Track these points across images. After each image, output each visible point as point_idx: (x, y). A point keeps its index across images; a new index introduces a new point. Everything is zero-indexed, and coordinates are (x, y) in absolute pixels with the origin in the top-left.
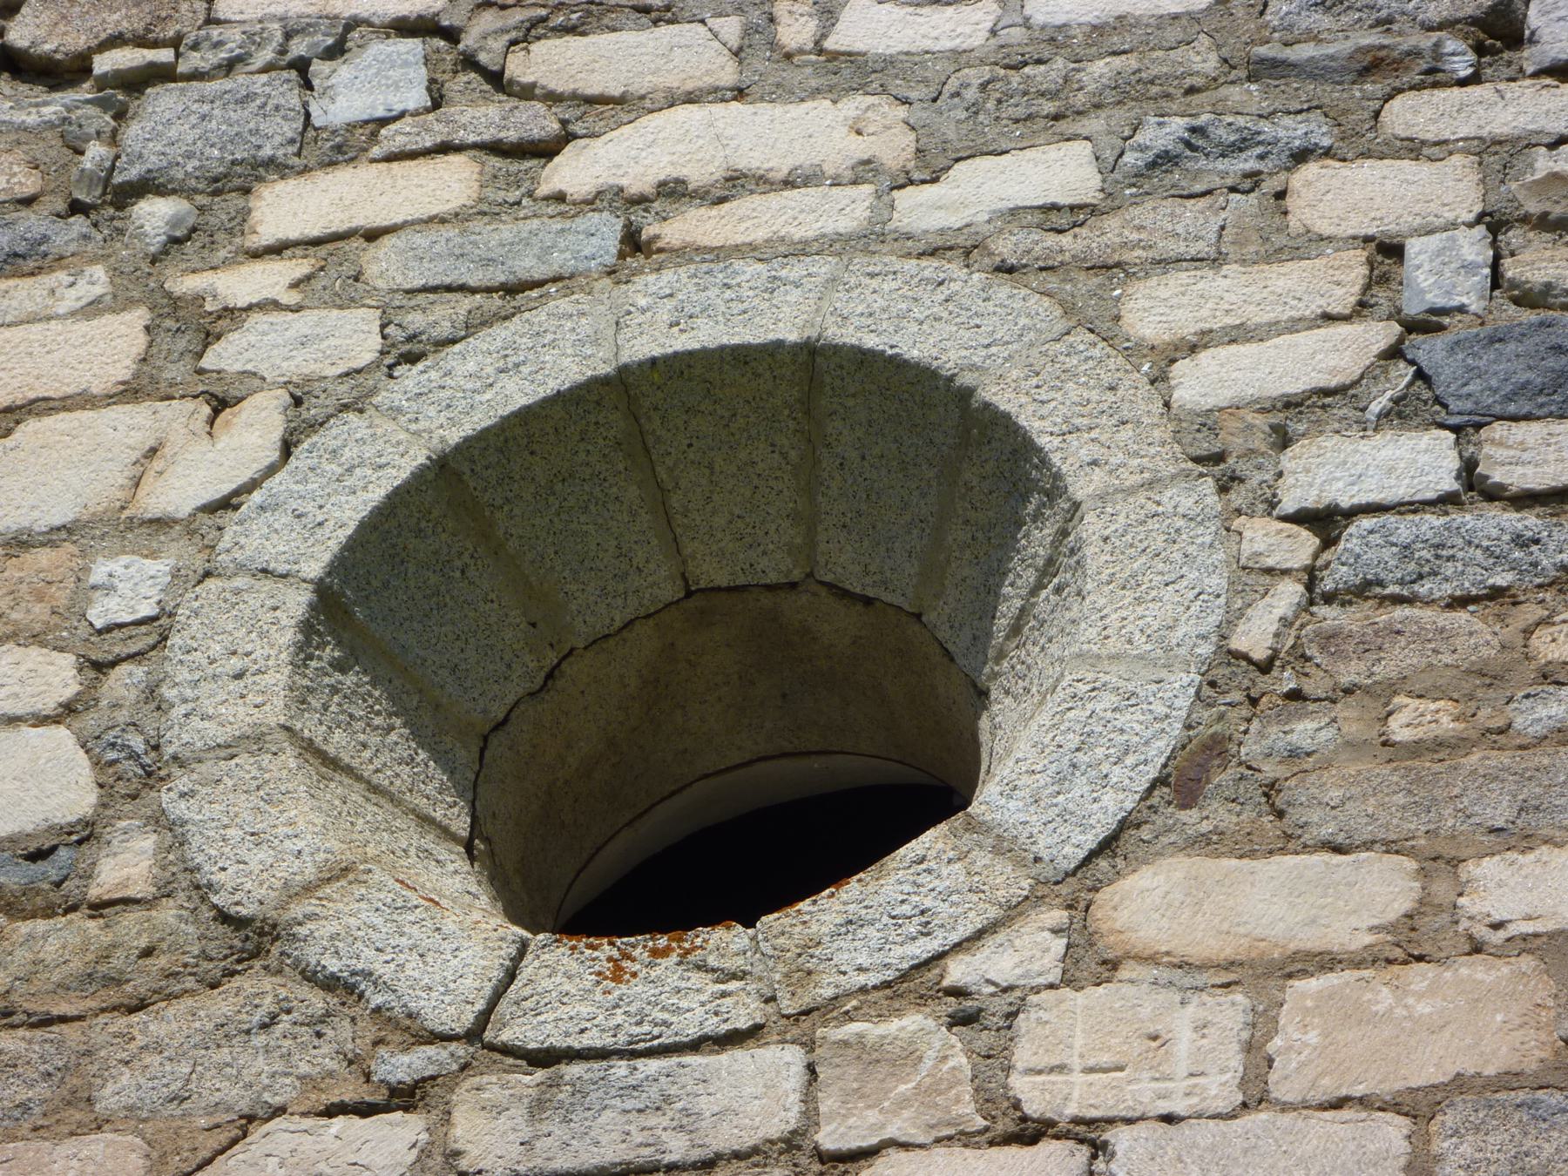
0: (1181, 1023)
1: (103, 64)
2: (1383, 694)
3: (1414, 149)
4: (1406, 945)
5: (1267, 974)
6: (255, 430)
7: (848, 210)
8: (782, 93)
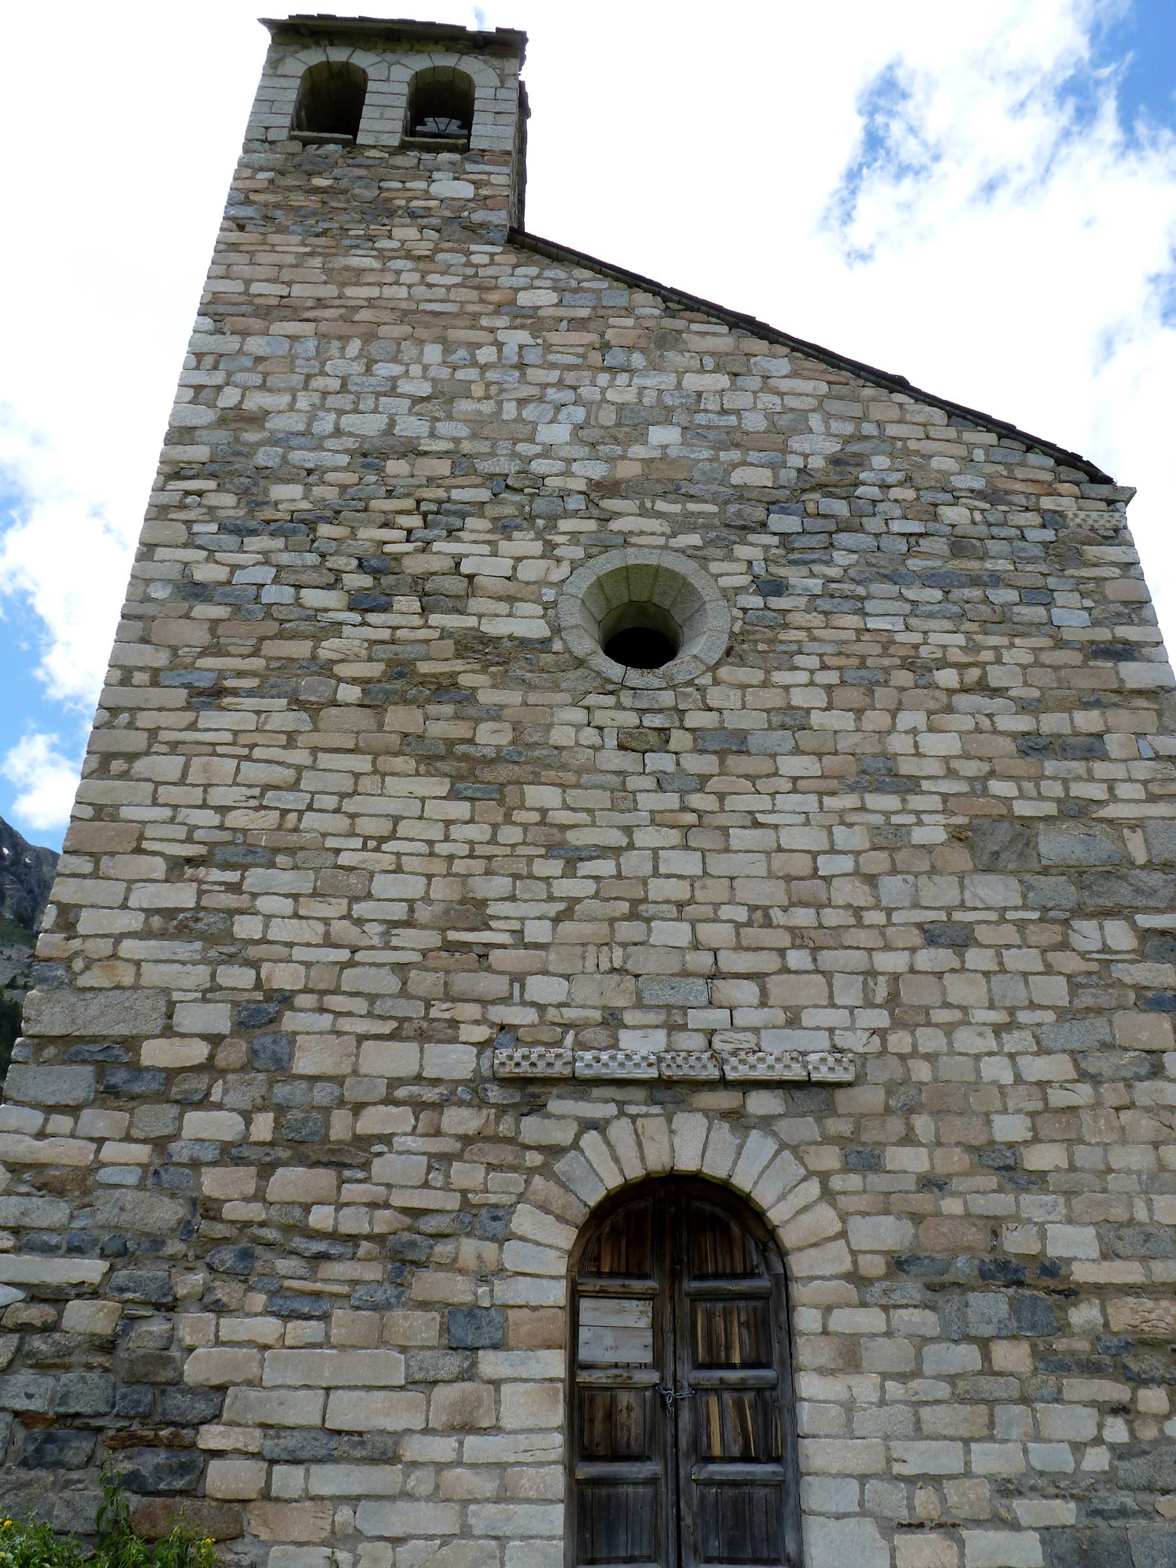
0: (731, 693)
1: (527, 491)
2: (756, 642)
3: (752, 544)
4: (765, 684)
5: (743, 687)
6: (565, 569)
7: (661, 541)
8: (647, 517)
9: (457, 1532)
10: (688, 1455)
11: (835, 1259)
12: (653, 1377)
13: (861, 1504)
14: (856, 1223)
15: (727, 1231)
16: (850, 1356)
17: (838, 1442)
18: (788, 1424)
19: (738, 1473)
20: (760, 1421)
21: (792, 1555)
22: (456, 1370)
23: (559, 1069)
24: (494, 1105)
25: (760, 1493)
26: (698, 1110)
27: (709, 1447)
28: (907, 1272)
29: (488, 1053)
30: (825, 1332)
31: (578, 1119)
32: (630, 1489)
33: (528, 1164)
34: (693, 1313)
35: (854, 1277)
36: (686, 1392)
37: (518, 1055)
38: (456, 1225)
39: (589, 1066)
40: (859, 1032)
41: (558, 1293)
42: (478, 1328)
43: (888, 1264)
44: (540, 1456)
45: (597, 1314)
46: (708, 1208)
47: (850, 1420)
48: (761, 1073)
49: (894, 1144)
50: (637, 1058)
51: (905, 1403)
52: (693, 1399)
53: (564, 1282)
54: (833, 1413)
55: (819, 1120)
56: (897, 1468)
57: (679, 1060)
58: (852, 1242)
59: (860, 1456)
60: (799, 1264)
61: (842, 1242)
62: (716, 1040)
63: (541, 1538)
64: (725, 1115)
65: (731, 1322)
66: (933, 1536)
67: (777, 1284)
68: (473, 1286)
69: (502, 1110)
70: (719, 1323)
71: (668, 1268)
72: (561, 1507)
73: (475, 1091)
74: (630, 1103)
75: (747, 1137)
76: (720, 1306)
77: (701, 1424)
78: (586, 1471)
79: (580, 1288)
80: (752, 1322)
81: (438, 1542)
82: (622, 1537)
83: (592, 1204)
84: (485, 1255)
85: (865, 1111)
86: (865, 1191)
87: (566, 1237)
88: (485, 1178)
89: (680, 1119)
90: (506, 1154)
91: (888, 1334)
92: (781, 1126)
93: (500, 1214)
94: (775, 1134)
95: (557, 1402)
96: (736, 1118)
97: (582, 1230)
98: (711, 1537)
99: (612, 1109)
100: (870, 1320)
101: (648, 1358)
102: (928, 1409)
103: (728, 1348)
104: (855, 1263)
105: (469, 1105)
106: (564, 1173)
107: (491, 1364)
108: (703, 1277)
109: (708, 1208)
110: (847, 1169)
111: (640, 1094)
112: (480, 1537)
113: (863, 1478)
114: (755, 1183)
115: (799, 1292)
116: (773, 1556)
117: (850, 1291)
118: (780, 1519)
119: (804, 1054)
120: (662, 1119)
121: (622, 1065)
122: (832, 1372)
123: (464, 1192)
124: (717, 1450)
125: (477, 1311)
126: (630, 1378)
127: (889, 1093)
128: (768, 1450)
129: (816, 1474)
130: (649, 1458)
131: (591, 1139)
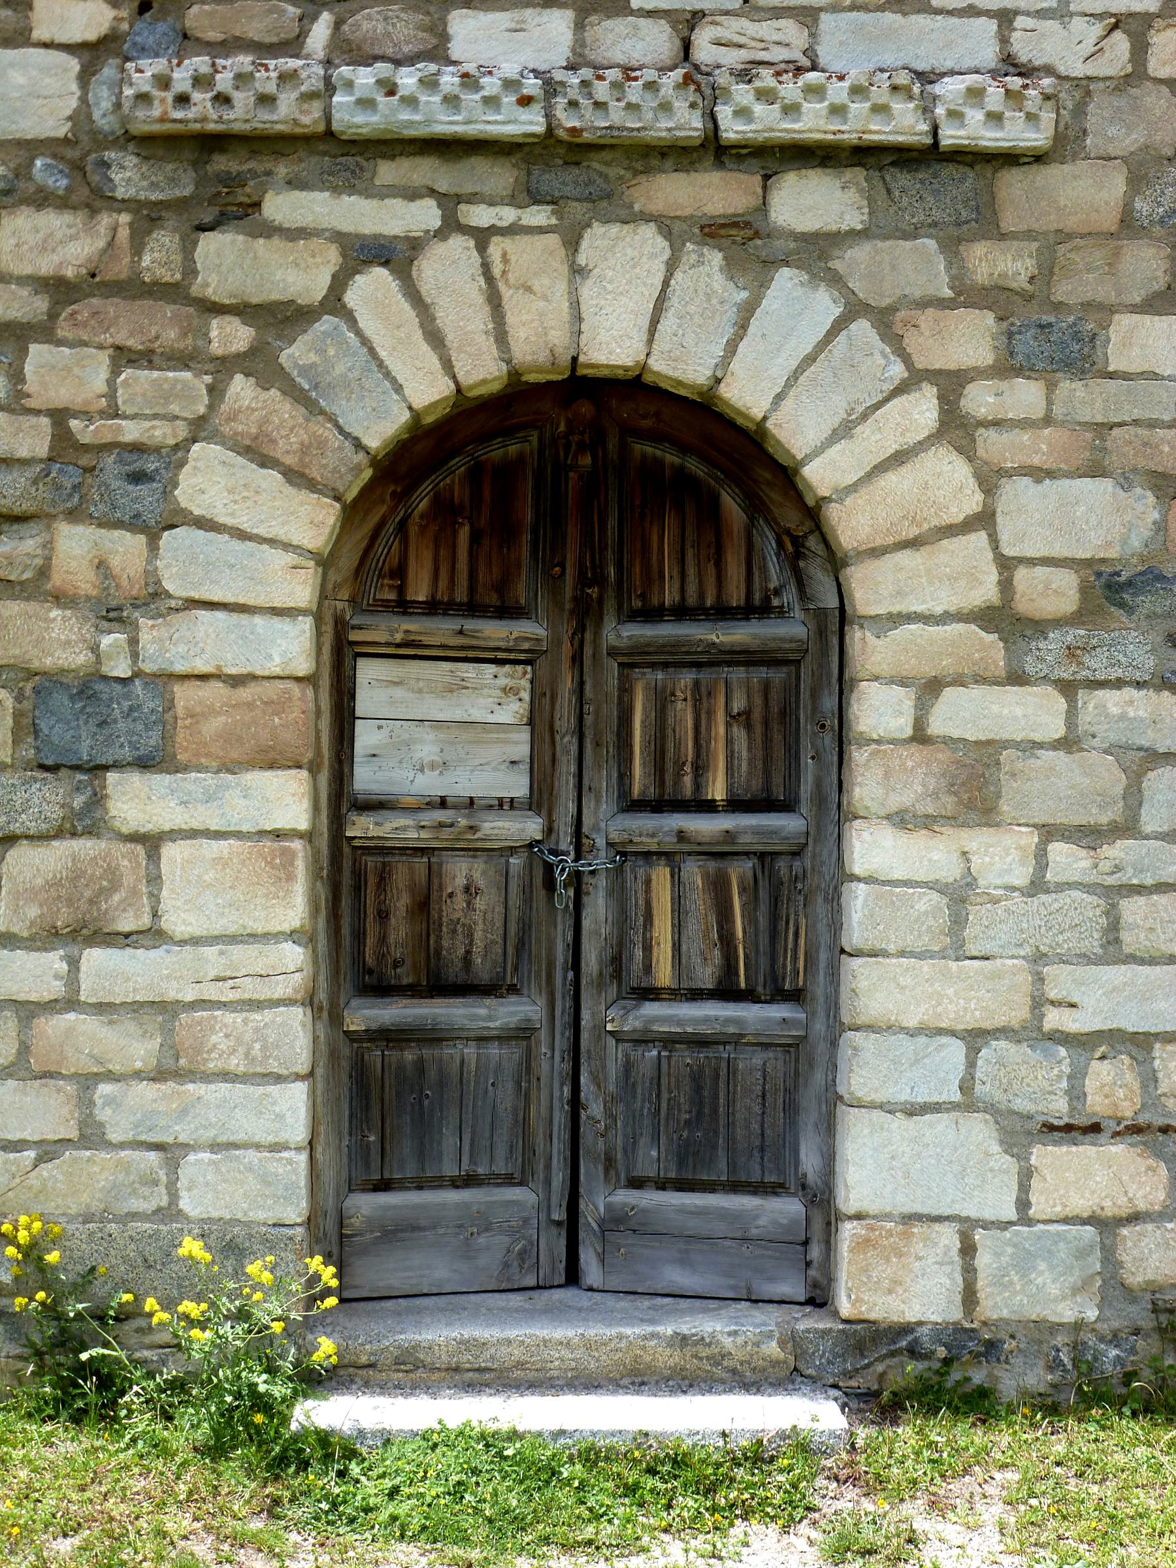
9: (74, 1134)
10: (600, 985)
11: (960, 576)
12: (531, 827)
13: (966, 1087)
14: (1019, 494)
15: (711, 513)
16: (974, 786)
17: (926, 966)
18: (822, 927)
19: (706, 1020)
20: (763, 920)
21: (812, 1178)
22: (55, 813)
23: (289, 114)
24: (125, 205)
25: (751, 1062)
26: (646, 217)
27: (648, 968)
28: (1130, 610)
29: (109, 71)
30: (920, 736)
31: (339, 238)
32: (470, 1051)
33: (216, 348)
34: (626, 690)
35: (1003, 618)
36: (600, 860)
37: (181, 78)
38: (43, 492)
39: (366, 103)
40: (1078, 23)
41: (291, 647)
42: (102, 724)
43: (1085, 590)
44: (251, 989)
45: (399, 693)
46: (671, 458)
47: (958, 921)
48: (813, 123)
49: (1135, 309)
50: (490, 85)
51: (1088, 888)
52: (619, 870)
53: (306, 624)
54: (922, 906)
55: (952, 247)
56: (1054, 1019)
57: (601, 90)
58: (1004, 536)
59: (980, 993)
60: (871, 588)
61: (980, 539)
62: (703, 39)
63: (258, 1147)
64: (713, 231)
65: (710, 713)
66: (1118, 1149)
67: (822, 633)
68: (87, 630)
69: (149, 217)
70: (683, 714)
71: (568, 592)
72: (300, 1091)
73: (78, 167)
74: (473, 198)
75: (763, 285)
76: (686, 678)
77: (631, 922)
78: (364, 1015)
79: (354, 636)
80: (757, 715)
81: (31, 1154)
82: (449, 1142)
83: (373, 442)
84: (115, 562)
85: (1071, 223)
86: (1048, 420)
87: (312, 521)
88: (111, 383)
89: (598, 240)
90: (164, 326)
91: (1069, 743)
92: (855, 261)
93: (151, 467)
94: (836, 280)
95: (291, 878)
96: (745, 242)
97: (352, 512)
98: (644, 1141)
99: (424, 215)
100: (1033, 712)
101: (518, 786)
102: (1141, 901)
103: (700, 768)
104: (1006, 585)
105: (63, 203)
106: (305, 370)
107: (134, 800)
108: (651, 614)
109: (671, 458)
110: (1008, 367)
111: (499, 176)
112: (122, 1146)
113: (975, 1039)
114: (779, 398)
115: (870, 651)
116: (771, 1178)
117: (989, 647)
118: (791, 1108)
119: (927, 77)
120: (553, 240)
121: (452, 101)
122: (928, 823)
123: (59, 416)
124: (664, 975)
125: (99, 687)
126: (472, 828)
127: (1137, 181)
128: (775, 978)
129: (870, 1028)
130: (513, 990)
131: (372, 289)
